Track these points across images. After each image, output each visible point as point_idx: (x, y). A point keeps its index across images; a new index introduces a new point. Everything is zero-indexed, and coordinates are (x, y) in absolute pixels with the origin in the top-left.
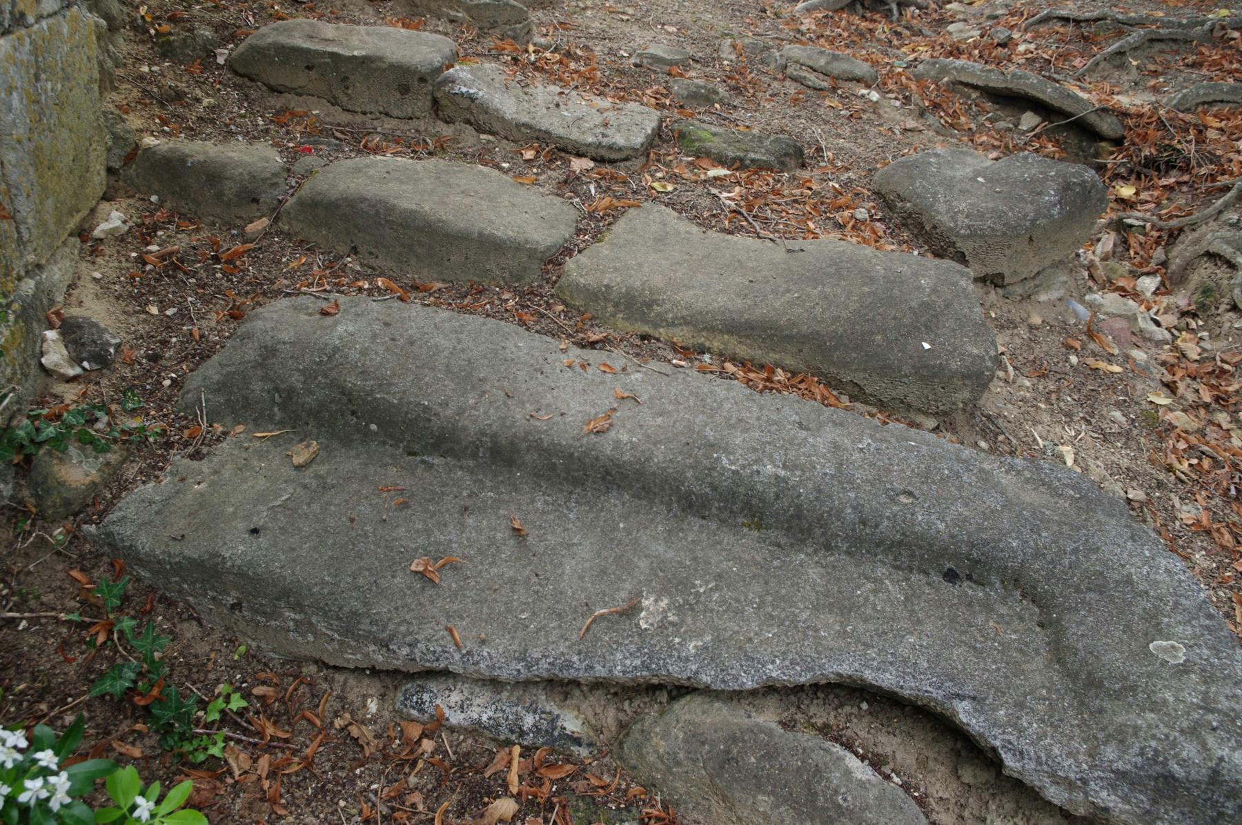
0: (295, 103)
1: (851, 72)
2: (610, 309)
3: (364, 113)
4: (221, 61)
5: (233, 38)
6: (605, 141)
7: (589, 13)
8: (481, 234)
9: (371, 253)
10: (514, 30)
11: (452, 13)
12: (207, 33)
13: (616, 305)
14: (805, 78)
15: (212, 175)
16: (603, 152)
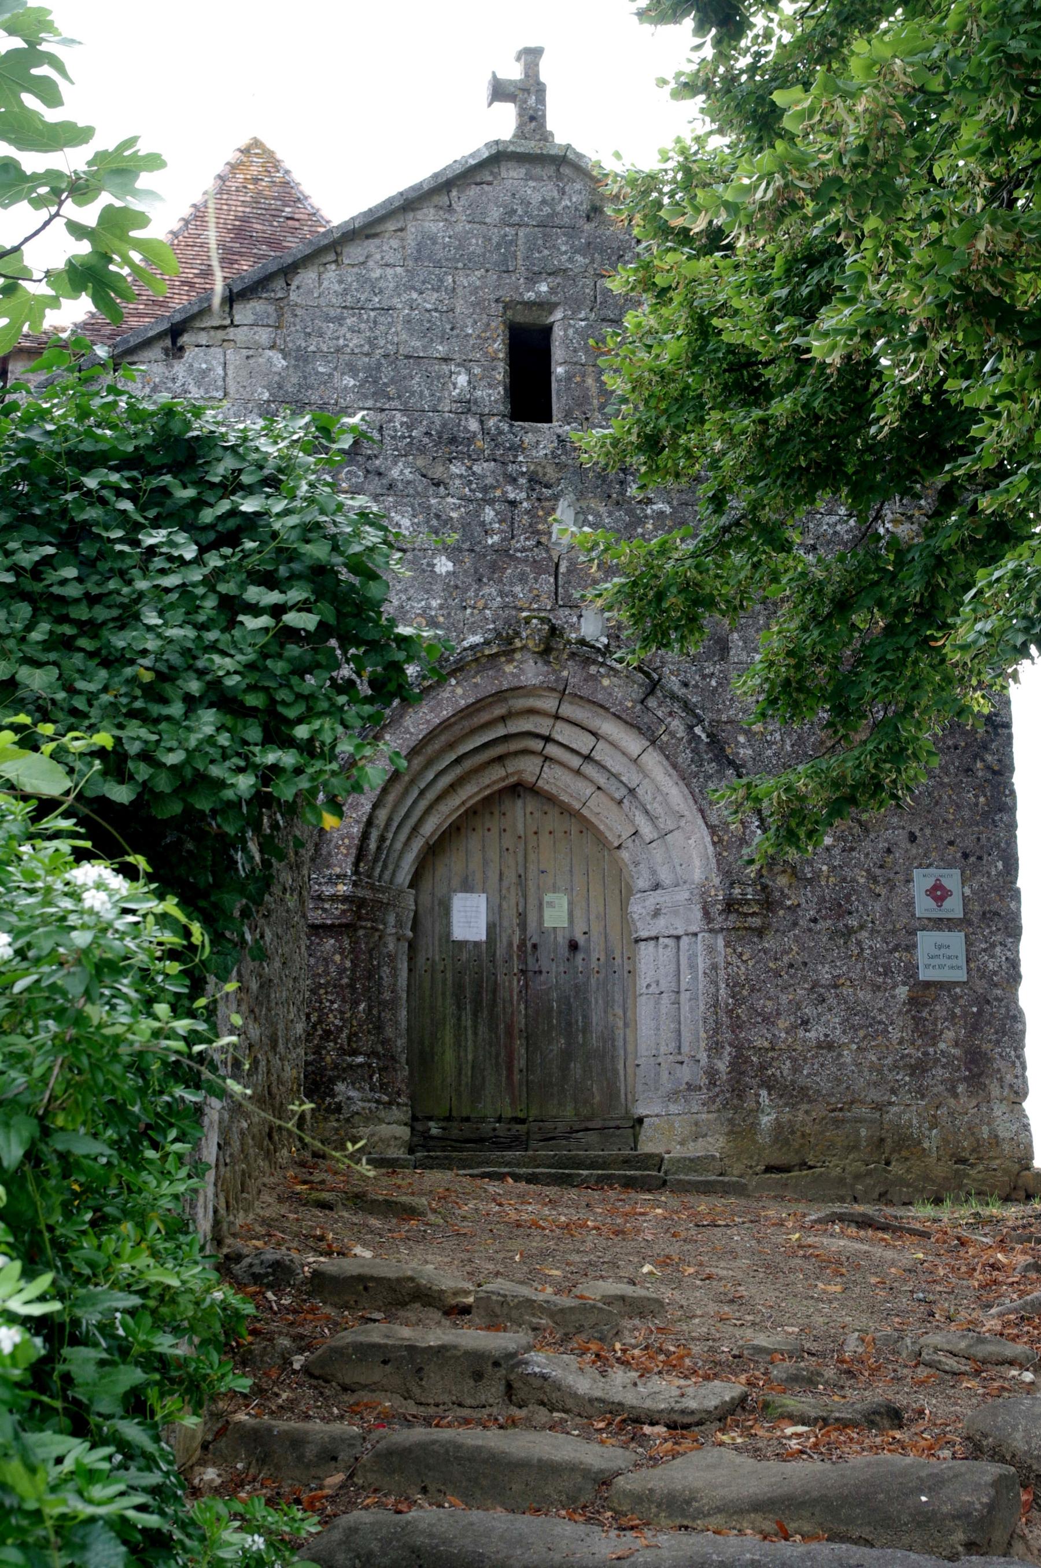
0: (365, 1396)
1: (999, 1354)
2: (654, 1510)
3: (437, 1405)
4: (297, 1366)
5: (309, 1347)
6: (677, 1407)
7: (697, 1321)
8: (540, 1460)
9: (440, 1491)
10: (601, 1332)
11: (535, 1320)
12: (285, 1342)
13: (659, 1506)
14: (940, 1362)
15: (296, 1442)
16: (675, 1417)
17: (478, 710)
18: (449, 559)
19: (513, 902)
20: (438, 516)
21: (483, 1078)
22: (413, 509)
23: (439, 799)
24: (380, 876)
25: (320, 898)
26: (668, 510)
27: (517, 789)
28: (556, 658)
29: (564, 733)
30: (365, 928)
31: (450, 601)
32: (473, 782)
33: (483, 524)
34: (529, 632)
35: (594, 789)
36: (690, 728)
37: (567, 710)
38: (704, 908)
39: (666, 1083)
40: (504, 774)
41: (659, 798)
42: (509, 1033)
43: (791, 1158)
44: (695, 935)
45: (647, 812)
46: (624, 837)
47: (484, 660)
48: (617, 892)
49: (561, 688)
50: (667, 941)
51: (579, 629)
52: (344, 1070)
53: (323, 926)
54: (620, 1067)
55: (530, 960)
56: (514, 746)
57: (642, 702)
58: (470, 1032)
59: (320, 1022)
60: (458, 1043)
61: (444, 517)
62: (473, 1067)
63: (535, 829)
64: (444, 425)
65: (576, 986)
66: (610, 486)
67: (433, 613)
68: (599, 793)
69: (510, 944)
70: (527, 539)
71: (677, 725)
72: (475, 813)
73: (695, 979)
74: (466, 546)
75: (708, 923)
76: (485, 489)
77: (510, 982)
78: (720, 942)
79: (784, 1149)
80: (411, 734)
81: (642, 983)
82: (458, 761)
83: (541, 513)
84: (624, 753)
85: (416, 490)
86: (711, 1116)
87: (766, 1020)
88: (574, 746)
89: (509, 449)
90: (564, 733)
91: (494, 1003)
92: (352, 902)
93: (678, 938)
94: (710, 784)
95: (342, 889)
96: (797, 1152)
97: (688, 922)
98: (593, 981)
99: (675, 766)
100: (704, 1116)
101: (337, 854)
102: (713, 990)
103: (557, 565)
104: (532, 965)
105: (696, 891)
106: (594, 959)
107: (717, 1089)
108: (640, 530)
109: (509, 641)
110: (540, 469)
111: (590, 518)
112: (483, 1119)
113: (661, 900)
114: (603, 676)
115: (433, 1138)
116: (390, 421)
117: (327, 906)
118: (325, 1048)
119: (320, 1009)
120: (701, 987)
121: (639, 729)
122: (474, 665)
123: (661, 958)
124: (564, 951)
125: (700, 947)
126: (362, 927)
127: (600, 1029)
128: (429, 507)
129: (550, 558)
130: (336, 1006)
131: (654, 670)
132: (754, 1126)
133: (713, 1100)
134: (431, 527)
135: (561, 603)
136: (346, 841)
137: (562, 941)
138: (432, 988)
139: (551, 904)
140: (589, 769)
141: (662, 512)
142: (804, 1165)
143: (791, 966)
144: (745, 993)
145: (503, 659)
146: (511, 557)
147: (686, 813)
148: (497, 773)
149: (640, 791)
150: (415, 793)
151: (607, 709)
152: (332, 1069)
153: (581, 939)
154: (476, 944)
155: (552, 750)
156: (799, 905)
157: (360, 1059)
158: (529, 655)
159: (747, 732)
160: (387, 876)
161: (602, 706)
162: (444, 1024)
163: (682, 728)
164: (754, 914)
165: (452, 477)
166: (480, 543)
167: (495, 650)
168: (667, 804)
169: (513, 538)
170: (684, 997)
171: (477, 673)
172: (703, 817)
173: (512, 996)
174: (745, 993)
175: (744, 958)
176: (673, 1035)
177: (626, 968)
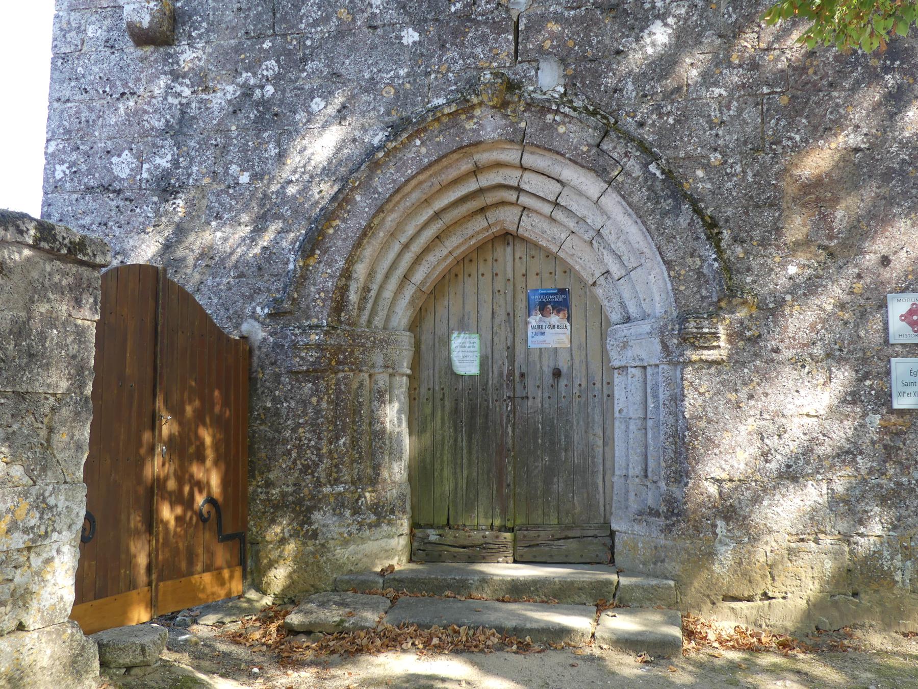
18: (415, 30)
19: (503, 339)
23: (427, 250)
24: (369, 322)
27: (507, 237)
29: (531, 182)
31: (416, 69)
32: (458, 233)
36: (646, 166)
37: (529, 160)
38: (662, 342)
39: (634, 506)
44: (657, 366)
46: (597, 275)
47: (445, 120)
48: (598, 324)
49: (519, 138)
50: (633, 370)
55: (518, 387)
56: (491, 198)
58: (465, 451)
68: (572, 236)
80: (379, 193)
82: (437, 215)
90: (531, 182)
93: (644, 368)
100: (663, 542)
101: (315, 307)
106: (576, 385)
114: (559, 124)
115: (430, 543)
117: (303, 354)
121: (596, 172)
124: (548, 379)
129: (510, 18)
130: (313, 443)
131: (610, 114)
137: (547, 371)
140: (559, 215)
145: (463, 117)
146: (472, 20)
147: (645, 250)
148: (479, 223)
150: (397, 247)
151: (563, 155)
152: (309, 500)
153: (564, 368)
155: (525, 200)
156: (760, 336)
159: (707, 167)
160: (378, 321)
163: (638, 167)
170: (650, 423)
173: (501, 420)
177: (606, 392)
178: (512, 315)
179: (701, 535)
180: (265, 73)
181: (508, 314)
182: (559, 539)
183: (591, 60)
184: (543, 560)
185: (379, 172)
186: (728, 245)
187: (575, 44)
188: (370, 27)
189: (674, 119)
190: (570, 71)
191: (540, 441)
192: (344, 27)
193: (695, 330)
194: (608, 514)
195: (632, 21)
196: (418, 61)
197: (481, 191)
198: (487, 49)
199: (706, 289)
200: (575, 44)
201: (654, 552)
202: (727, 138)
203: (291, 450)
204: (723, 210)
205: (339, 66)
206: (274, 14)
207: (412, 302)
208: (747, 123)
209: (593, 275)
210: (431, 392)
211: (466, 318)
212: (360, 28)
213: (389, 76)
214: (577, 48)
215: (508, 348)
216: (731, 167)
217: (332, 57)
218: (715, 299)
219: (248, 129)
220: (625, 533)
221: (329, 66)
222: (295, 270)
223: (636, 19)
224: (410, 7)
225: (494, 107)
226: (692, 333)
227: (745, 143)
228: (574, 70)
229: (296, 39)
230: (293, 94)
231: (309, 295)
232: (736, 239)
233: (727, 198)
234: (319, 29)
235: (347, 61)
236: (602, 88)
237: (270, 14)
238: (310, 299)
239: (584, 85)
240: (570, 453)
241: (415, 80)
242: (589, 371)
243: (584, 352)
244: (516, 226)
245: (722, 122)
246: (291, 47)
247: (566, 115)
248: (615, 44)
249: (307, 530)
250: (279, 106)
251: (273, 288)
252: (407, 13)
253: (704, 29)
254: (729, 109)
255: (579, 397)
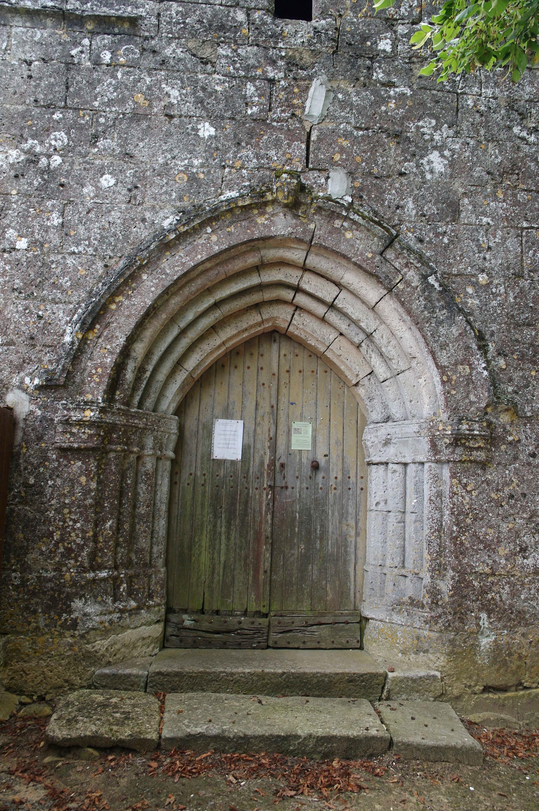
17: (233, 258)
18: (212, 125)
19: (266, 428)
20: (204, 89)
21: (233, 578)
22: (182, 82)
24: (140, 405)
25: (67, 422)
26: (409, 92)
28: (304, 213)
30: (115, 451)
32: (233, 325)
33: (244, 97)
34: (279, 184)
35: (337, 334)
36: (424, 278)
39: (391, 594)
40: (260, 319)
41: (393, 342)
42: (257, 539)
43: (510, 680)
44: (422, 463)
45: (381, 355)
46: (361, 376)
48: (354, 422)
49: (308, 239)
50: (396, 467)
51: (326, 189)
52: (82, 587)
53: (70, 449)
54: (351, 570)
55: (278, 477)
56: (269, 295)
57: (381, 254)
58: (223, 537)
59: (62, 540)
60: (212, 546)
61: (209, 90)
62: (224, 568)
63: (287, 368)
64: (215, 15)
65: (316, 500)
66: (358, 71)
67: (195, 171)
68: (341, 338)
69: (262, 463)
70: (283, 111)
71: (412, 276)
72: (238, 353)
73: (420, 502)
74: (228, 114)
75: (436, 454)
76: (248, 69)
77: (261, 496)
78: (446, 472)
79: (502, 671)
80: (167, 274)
81: (372, 501)
82: (216, 305)
83: (296, 90)
84: (363, 302)
85: (185, 66)
86: (432, 634)
87: (488, 546)
88: (319, 294)
89: (271, 37)
91: (245, 514)
92: (98, 427)
93: (405, 465)
94: (441, 329)
95: (89, 414)
96: (514, 673)
97: (416, 452)
98: (331, 496)
99: (409, 312)
100: (426, 633)
101: (90, 382)
102: (437, 515)
103: (309, 135)
104: (279, 482)
105: (424, 425)
107: (440, 610)
108: (383, 108)
109: (262, 195)
110: (297, 55)
111: (340, 96)
112: (231, 613)
113: (390, 431)
114: (346, 230)
115: (185, 628)
116: (167, 10)
117: (75, 430)
118: (66, 565)
119: (64, 528)
120: (426, 512)
122: (228, 216)
123: (390, 482)
124: (307, 470)
125: (426, 476)
126: (112, 450)
127: (335, 537)
128: (197, 81)
129: (303, 128)
130: (78, 525)
131: (393, 227)
132: (475, 647)
133: (435, 619)
134: (197, 97)
135: (311, 166)
136: (100, 370)
137: (306, 461)
138: (193, 498)
139: (298, 431)
140: (333, 317)
141: (404, 94)
142: (519, 686)
143: (512, 497)
144: (468, 521)
145: (256, 212)
147: (417, 355)
148: (254, 318)
149: (376, 336)
150: (175, 332)
152: (71, 587)
153: (322, 461)
154: (233, 462)
155: (301, 299)
156: (519, 441)
157: (104, 574)
158: (279, 209)
159: (475, 284)
160: (149, 403)
161: (344, 257)
162: (202, 529)
163: (417, 278)
164: (479, 448)
165: (219, 57)
166: (240, 112)
167: (247, 202)
168: (401, 347)
169: (270, 110)
170: (410, 518)
171: (231, 223)
172: (434, 359)
173: (261, 508)
174: (468, 521)
175: (469, 488)
176: (399, 551)
177: (359, 486)
178: (275, 407)
179: (466, 627)
180: (53, 143)
181: (272, 407)
182: (312, 625)
183: (376, 178)
184: (296, 646)
185: (168, 253)
186: (493, 357)
187: (363, 161)
188: (166, 115)
189: (448, 240)
190: (357, 184)
191: (296, 529)
192: (141, 112)
193: (467, 432)
194: (358, 601)
195: (414, 148)
196: (212, 154)
197: (260, 287)
198: (281, 153)
199: (475, 395)
200: (363, 161)
201: (416, 642)
202: (493, 261)
203: (53, 532)
204: (489, 325)
205: (132, 147)
206: (67, 88)
207: (181, 388)
208: (510, 251)
209: (357, 375)
210: (192, 477)
211: (231, 407)
212: (156, 115)
213: (183, 164)
214: (364, 164)
215: (271, 439)
216: (496, 288)
217: (126, 138)
218: (483, 405)
219: (30, 196)
220: (381, 621)
221: (121, 146)
222: (73, 343)
223: (418, 147)
224: (208, 104)
225: (286, 206)
226: (465, 435)
227: (508, 268)
228: (361, 183)
229: (89, 116)
230: (82, 167)
231: (85, 370)
232: (500, 353)
233: (492, 314)
234: (114, 109)
235: (141, 144)
236: (386, 203)
237: (63, 87)
238: (86, 373)
239: (370, 198)
240: (325, 542)
241: (209, 172)
242: (346, 466)
243: (341, 447)
244: (287, 324)
245: (489, 248)
246: (82, 122)
247: (354, 222)
248: (398, 166)
249: (66, 620)
250: (66, 178)
251: (46, 359)
252: (204, 108)
253: (474, 164)
254: (495, 237)
255: (335, 489)
